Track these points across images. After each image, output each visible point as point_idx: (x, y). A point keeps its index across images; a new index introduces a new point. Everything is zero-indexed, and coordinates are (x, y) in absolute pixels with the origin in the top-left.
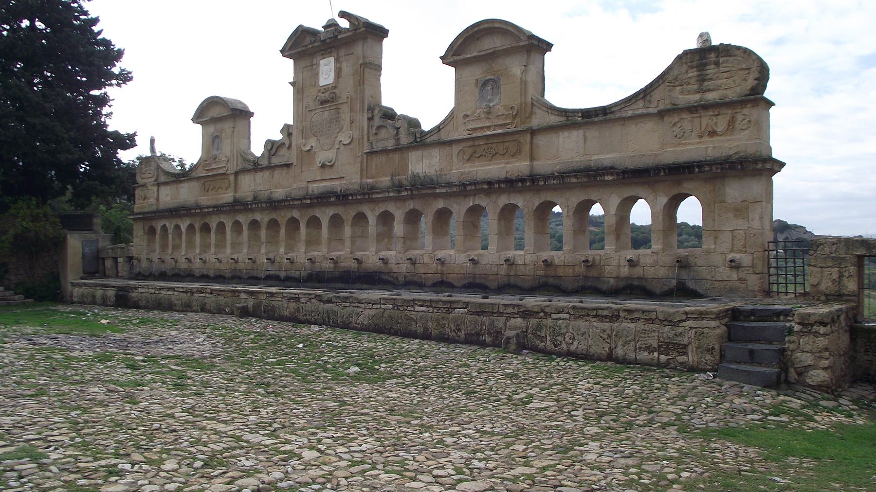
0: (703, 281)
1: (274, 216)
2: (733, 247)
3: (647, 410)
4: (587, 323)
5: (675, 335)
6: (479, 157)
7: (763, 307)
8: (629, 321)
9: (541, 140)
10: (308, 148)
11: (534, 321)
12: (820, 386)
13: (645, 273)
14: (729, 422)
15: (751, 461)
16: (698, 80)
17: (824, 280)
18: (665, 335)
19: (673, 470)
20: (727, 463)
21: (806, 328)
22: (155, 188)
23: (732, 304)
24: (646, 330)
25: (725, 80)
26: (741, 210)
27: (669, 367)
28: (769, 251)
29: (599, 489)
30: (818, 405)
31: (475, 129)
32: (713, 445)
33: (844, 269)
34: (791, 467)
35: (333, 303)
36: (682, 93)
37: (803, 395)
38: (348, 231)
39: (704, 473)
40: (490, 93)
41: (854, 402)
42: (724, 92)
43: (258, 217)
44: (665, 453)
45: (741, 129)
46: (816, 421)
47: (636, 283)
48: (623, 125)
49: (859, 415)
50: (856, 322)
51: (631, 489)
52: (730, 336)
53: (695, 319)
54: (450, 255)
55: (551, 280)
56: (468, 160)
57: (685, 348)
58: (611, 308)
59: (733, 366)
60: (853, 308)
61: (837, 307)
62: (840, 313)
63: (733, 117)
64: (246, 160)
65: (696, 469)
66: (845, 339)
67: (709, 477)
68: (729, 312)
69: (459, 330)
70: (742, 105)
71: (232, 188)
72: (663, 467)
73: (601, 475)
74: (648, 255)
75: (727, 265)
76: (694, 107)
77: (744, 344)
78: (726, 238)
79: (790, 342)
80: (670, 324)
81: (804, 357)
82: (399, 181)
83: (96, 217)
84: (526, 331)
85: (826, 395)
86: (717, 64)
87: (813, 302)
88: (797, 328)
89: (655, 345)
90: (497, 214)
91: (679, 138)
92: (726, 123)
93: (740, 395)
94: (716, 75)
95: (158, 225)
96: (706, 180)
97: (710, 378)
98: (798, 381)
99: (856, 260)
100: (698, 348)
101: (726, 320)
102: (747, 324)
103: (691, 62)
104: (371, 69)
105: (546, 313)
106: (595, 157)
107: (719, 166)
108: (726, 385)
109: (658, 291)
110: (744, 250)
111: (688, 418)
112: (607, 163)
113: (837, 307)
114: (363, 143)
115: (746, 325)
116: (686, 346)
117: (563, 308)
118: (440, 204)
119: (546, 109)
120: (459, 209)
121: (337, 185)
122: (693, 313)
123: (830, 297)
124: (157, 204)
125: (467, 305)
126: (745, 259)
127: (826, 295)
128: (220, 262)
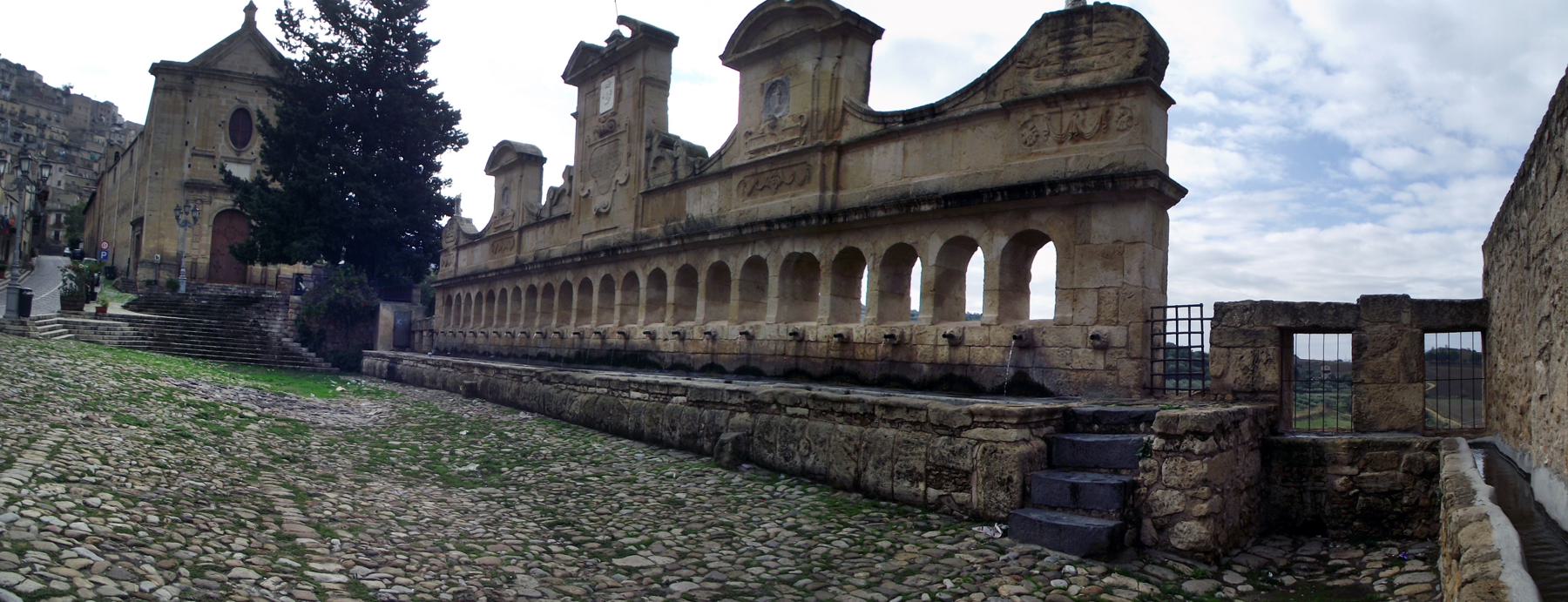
0: (1055, 371)
1: (549, 280)
2: (1099, 316)
4: (830, 425)
5: (952, 452)
6: (762, 190)
8: (888, 425)
9: (851, 161)
10: (586, 192)
11: (763, 417)
12: (1193, 550)
16: (1061, 58)
17: (1231, 369)
21: (1172, 444)
22: (455, 253)
24: (909, 442)
25: (1099, 57)
26: (1113, 256)
28: (1153, 322)
31: (758, 151)
33: (1261, 350)
35: (551, 384)
36: (1037, 77)
38: (618, 297)
40: (777, 101)
42: (1097, 74)
43: (535, 281)
45: (1118, 130)
47: (958, 372)
48: (957, 130)
52: (1052, 458)
53: (986, 425)
54: (722, 328)
55: (847, 366)
56: (750, 194)
58: (863, 401)
62: (1240, 417)
63: (1108, 112)
64: (531, 214)
66: (1250, 464)
68: (1056, 417)
69: (674, 429)
70: (1120, 92)
71: (515, 248)
74: (977, 328)
76: (1052, 95)
79: (1145, 470)
80: (947, 432)
81: (1167, 498)
82: (675, 229)
83: (416, 288)
84: (752, 434)
85: (1202, 567)
86: (1089, 33)
88: (1157, 443)
89: (921, 468)
90: (779, 268)
91: (1030, 145)
92: (1097, 119)
94: (1087, 49)
95: (455, 293)
98: (1157, 543)
99: (1278, 334)
100: (985, 478)
103: (1053, 31)
104: (653, 86)
105: (779, 405)
106: (916, 180)
107: (1081, 185)
109: (988, 386)
112: (930, 188)
114: (639, 182)
115: (1078, 439)
116: (968, 474)
117: (800, 397)
118: (715, 257)
119: (859, 116)
120: (736, 263)
121: (611, 238)
122: (981, 415)
123: (1239, 396)
124: (455, 271)
125: (687, 391)
126: (1117, 335)
127: (1234, 393)
128: (500, 336)
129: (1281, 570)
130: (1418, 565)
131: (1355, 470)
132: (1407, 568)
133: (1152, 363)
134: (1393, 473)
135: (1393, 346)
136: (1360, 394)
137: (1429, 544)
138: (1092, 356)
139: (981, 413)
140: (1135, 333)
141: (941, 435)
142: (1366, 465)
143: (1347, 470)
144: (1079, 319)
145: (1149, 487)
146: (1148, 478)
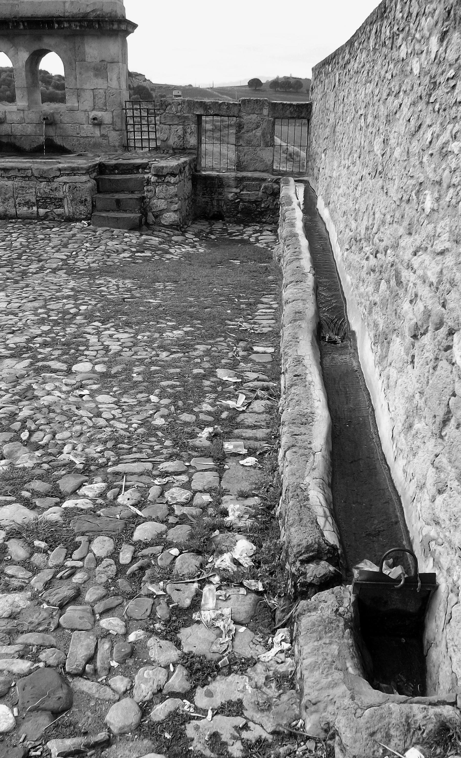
0: (70, 138)
2: (94, 106)
3: (37, 259)
5: (51, 190)
7: (125, 162)
8: (6, 179)
12: (172, 225)
13: (13, 130)
14: (106, 261)
15: (130, 290)
18: (42, 191)
19: (73, 306)
20: (112, 294)
23: (98, 159)
27: (48, 219)
29: (19, 330)
30: (170, 241)
32: (98, 282)
34: (159, 290)
37: (161, 234)
39: (97, 304)
41: (196, 235)
44: (63, 293)
46: (171, 253)
49: (201, 246)
50: (196, 171)
51: (45, 325)
53: (68, 175)
57: (61, 201)
59: (104, 214)
60: (194, 160)
61: (183, 160)
62: (185, 165)
65: (90, 302)
66: (189, 185)
67: (101, 307)
72: (64, 304)
73: (16, 319)
75: (90, 122)
77: (111, 195)
78: (88, 96)
79: (148, 191)
85: (176, 232)
87: (163, 155)
88: (153, 179)
89: (33, 200)
93: (112, 239)
96: (66, 37)
97: (85, 226)
100: (72, 201)
101: (95, 174)
102: (112, 177)
107: (77, 24)
108: (100, 231)
109: (27, 148)
110: (105, 108)
111: (73, 262)
113: (183, 160)
116: (61, 200)
123: (176, 151)
126: (106, 117)
127: (173, 149)
129: (208, 233)
130: (269, 233)
131: (238, 190)
132: (264, 234)
133: (127, 132)
134: (257, 192)
135: (258, 127)
136: (240, 151)
137: (273, 225)
138: (92, 128)
139: (65, 169)
140: (117, 116)
141: (41, 182)
142: (244, 188)
143: (234, 190)
144: (82, 107)
145: (150, 199)
146: (149, 194)
